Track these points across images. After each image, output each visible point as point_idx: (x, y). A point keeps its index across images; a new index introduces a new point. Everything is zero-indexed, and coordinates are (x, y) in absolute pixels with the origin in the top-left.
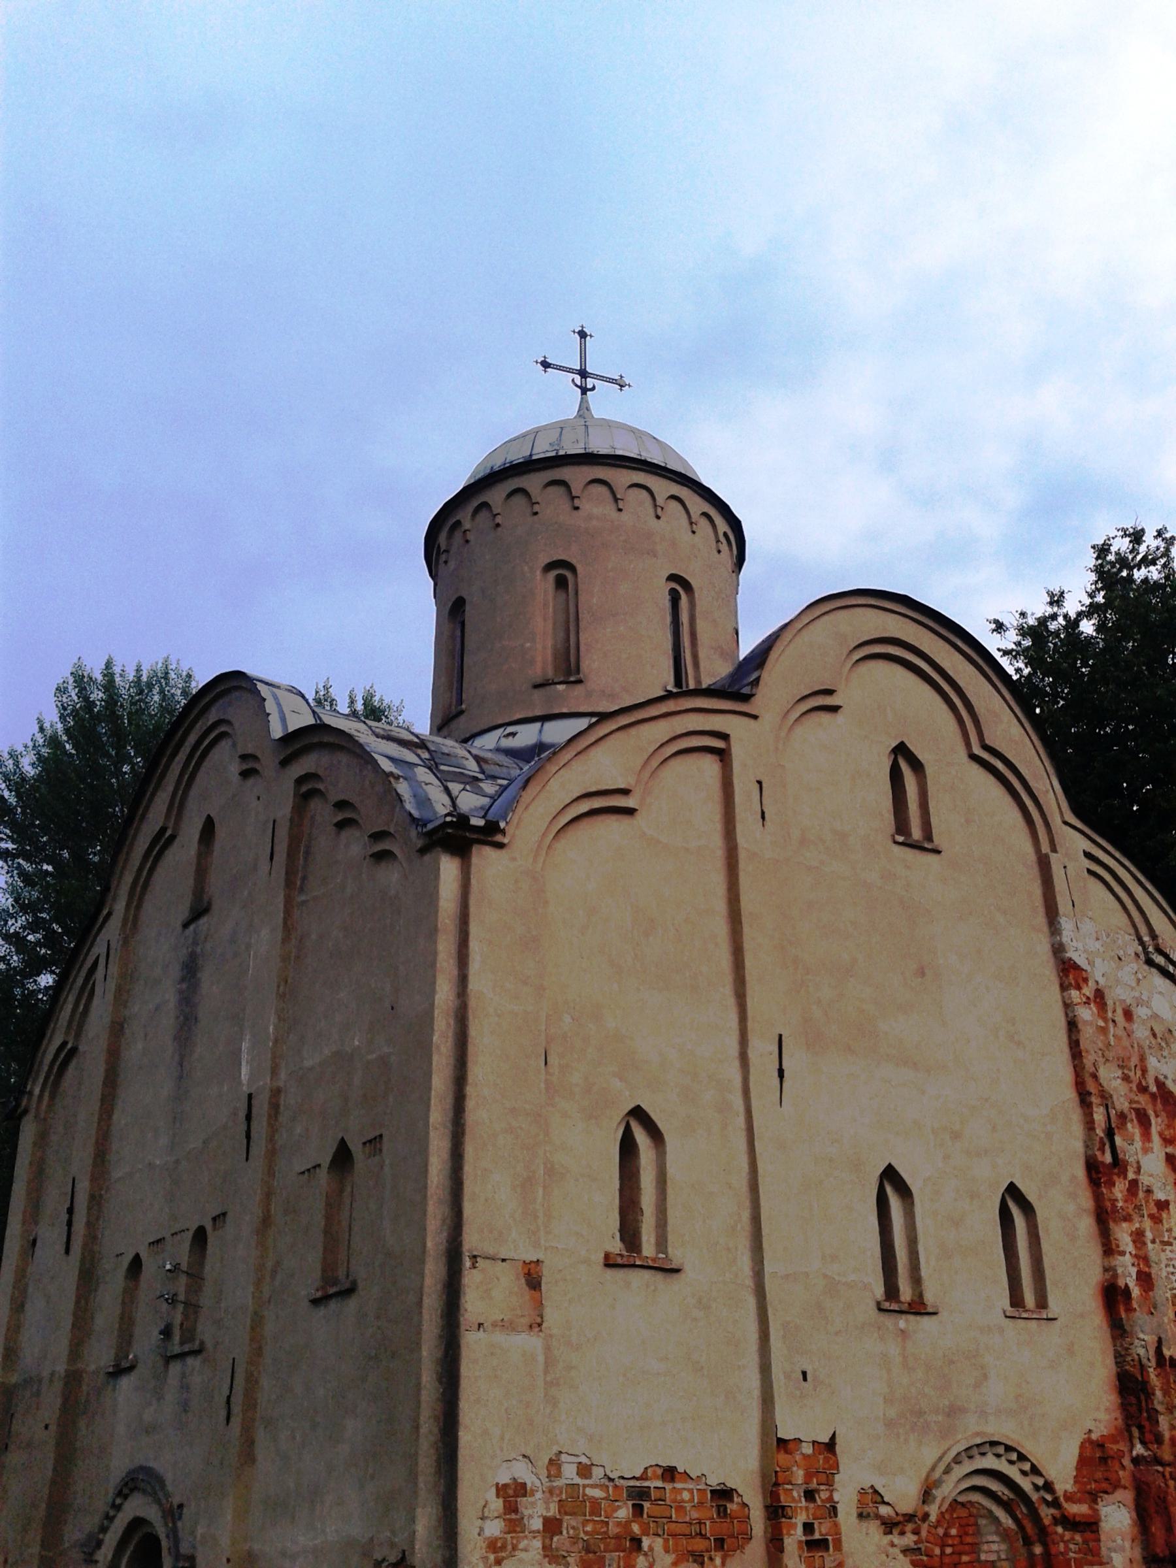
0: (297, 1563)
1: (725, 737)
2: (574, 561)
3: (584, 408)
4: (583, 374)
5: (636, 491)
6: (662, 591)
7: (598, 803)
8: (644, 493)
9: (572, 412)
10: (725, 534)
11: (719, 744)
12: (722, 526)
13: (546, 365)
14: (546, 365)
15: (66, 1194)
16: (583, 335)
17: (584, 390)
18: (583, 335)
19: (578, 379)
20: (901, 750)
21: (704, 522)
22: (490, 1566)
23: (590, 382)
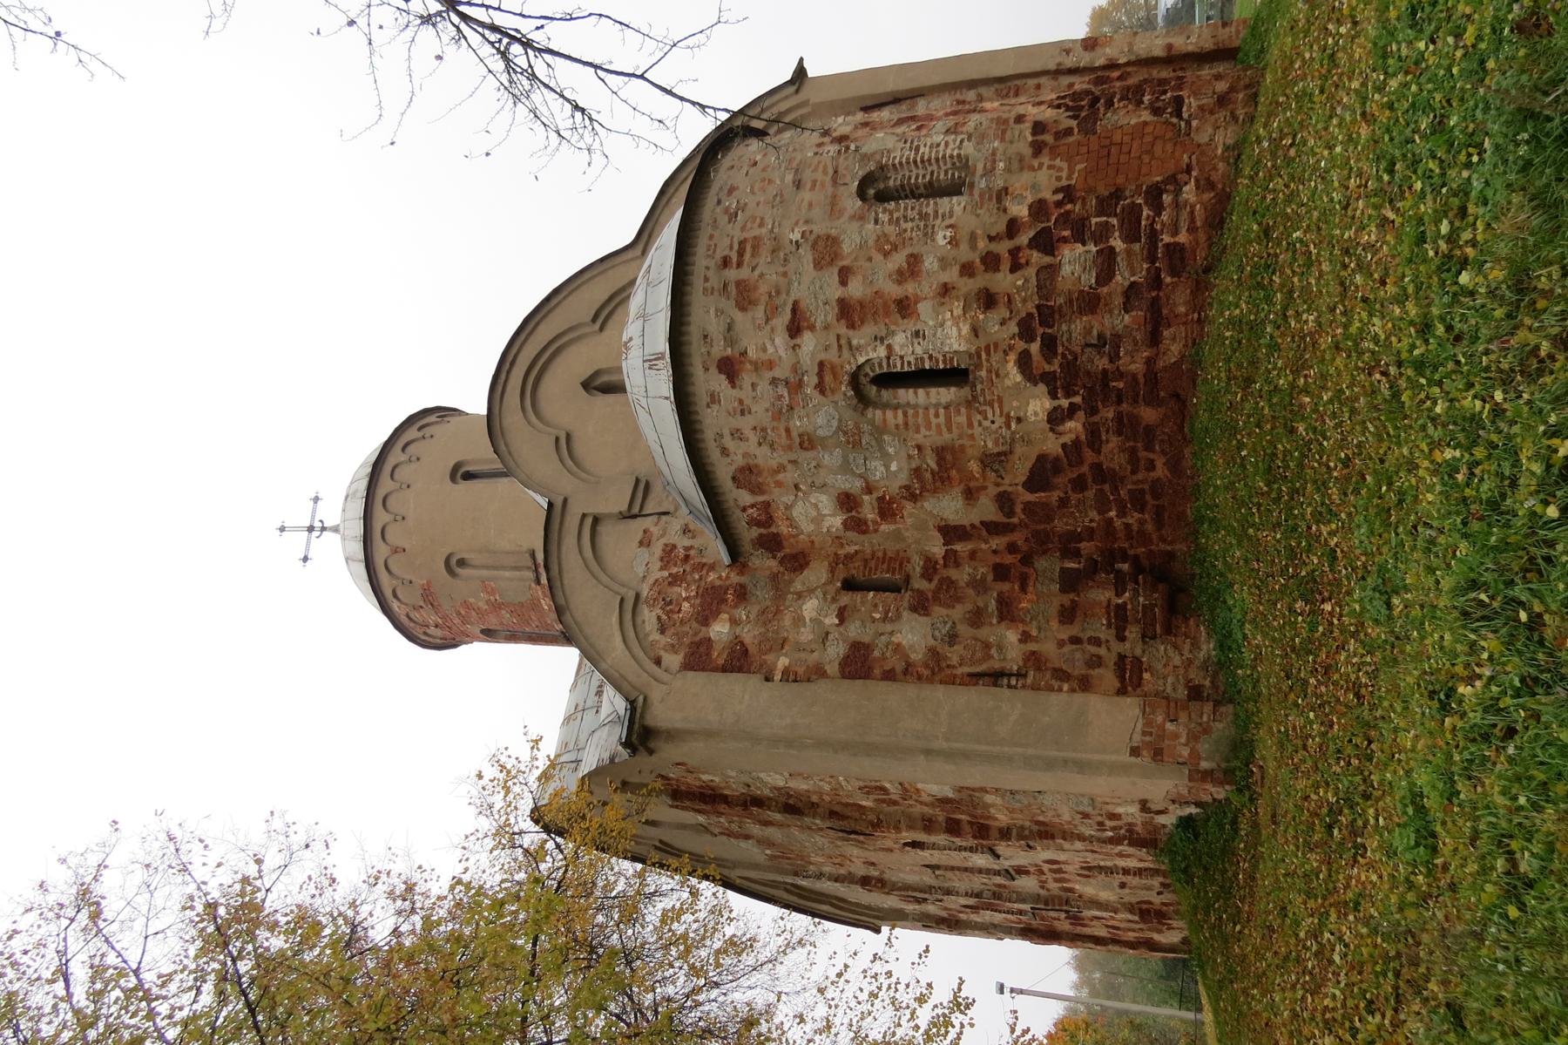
0: (1475, 979)
1: (584, 516)
2: (452, 464)
3: (335, 529)
4: (311, 529)
5: (387, 537)
6: (464, 486)
7: (628, 616)
8: (397, 471)
9: (336, 537)
10: (420, 429)
11: (589, 521)
12: (412, 433)
13: (316, 499)
14: (316, 499)
15: (661, 357)
16: (282, 529)
17: (323, 529)
18: (282, 529)
19: (315, 534)
20: (586, 385)
21: (411, 449)
22: (1566, 885)
23: (317, 524)
